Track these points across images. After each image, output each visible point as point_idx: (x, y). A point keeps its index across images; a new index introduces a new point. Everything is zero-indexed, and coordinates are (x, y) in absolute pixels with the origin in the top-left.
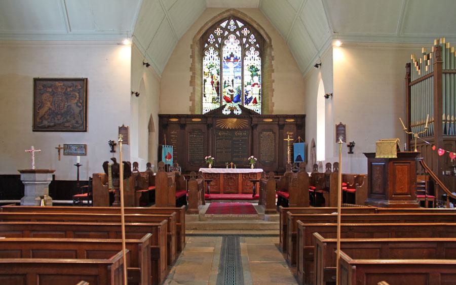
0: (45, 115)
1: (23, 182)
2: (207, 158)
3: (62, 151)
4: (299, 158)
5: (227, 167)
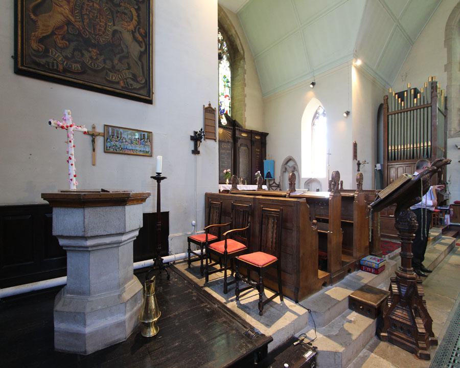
0: (53, 33)
1: (62, 242)
3: (100, 141)
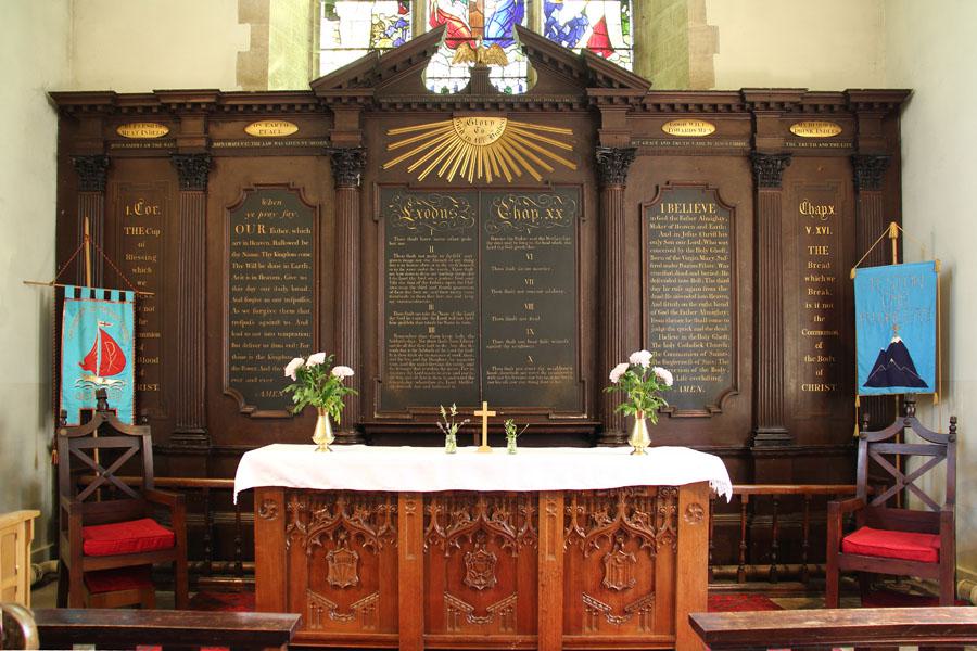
2: (300, 372)
4: (895, 363)
5: (451, 438)
